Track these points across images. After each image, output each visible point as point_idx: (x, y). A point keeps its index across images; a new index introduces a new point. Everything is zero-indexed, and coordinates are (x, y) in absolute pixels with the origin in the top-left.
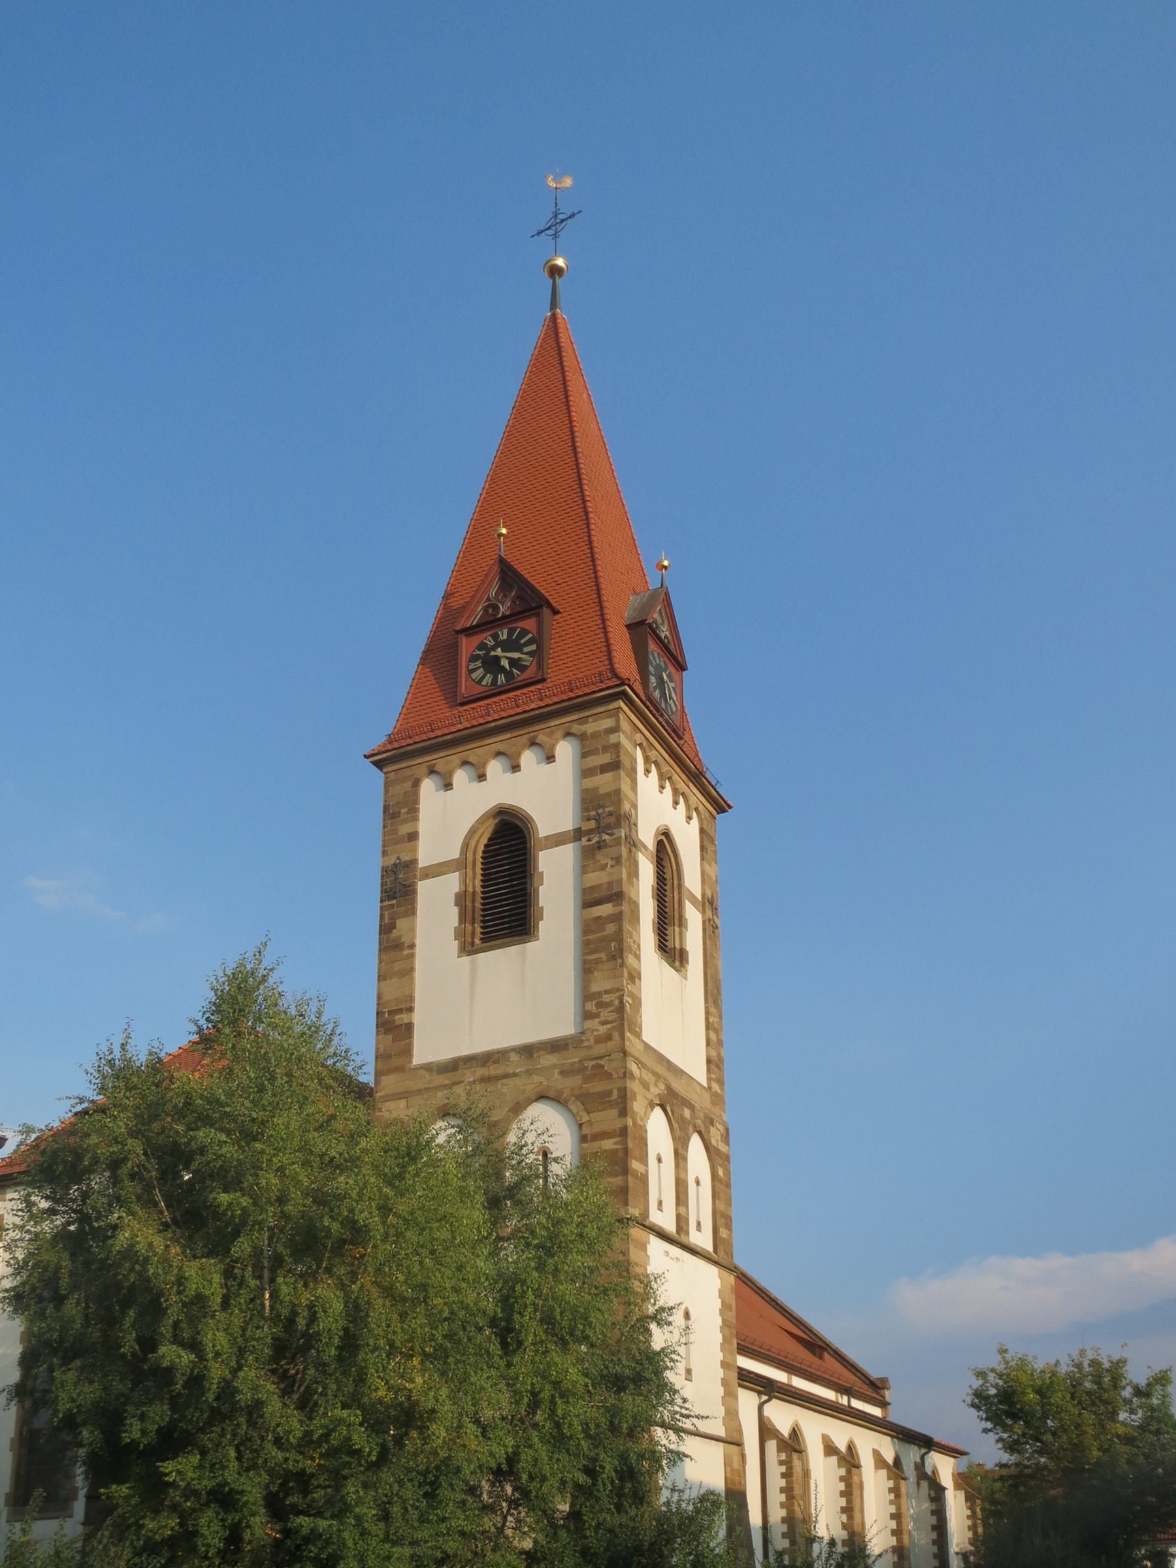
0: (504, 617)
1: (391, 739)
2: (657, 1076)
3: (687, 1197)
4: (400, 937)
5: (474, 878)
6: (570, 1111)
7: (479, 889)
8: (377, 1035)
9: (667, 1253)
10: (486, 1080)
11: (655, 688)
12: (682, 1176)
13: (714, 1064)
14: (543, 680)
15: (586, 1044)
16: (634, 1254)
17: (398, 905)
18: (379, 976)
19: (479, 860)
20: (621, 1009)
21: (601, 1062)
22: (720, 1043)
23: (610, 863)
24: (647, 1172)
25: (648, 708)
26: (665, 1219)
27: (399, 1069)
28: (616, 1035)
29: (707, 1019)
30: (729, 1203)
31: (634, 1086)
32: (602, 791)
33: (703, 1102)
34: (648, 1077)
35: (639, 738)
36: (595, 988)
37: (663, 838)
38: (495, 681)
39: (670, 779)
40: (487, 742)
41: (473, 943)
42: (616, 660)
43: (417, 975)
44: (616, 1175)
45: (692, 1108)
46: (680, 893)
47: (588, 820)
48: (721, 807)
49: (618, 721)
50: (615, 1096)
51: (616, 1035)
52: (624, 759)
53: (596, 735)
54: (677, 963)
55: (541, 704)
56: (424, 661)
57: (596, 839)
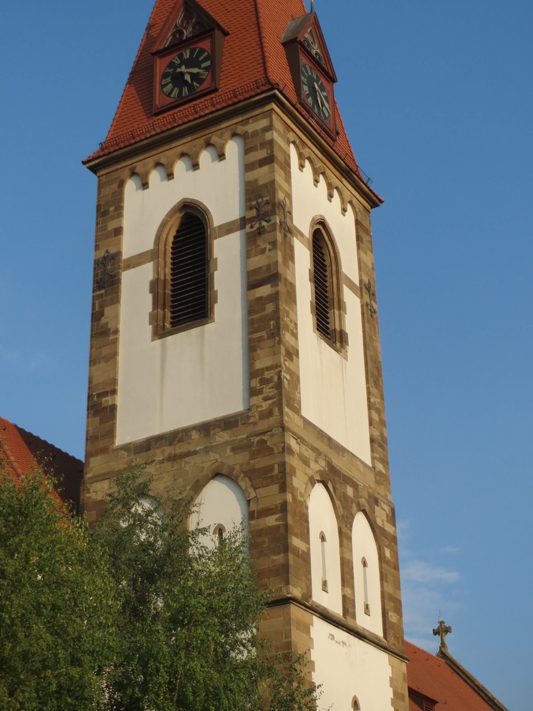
0: (188, 39)
1: (103, 147)
2: (318, 452)
3: (352, 578)
4: (106, 324)
5: (165, 267)
6: (240, 487)
7: (169, 277)
8: (88, 418)
9: (332, 637)
10: (172, 458)
11: (308, 96)
12: (347, 556)
13: (377, 443)
14: (216, 90)
15: (252, 420)
16: (296, 636)
17: (106, 294)
18: (90, 361)
19: (169, 250)
20: (279, 385)
21: (264, 437)
22: (382, 423)
23: (268, 247)
24: (309, 549)
25: (297, 110)
26: (331, 601)
27: (104, 451)
28: (276, 410)
29: (369, 399)
30: (397, 585)
31: (293, 461)
32: (260, 183)
33: (367, 481)
34: (308, 453)
35: (291, 136)
36: (259, 365)
37: (320, 227)
38: (180, 92)
39: (323, 174)
40: (174, 145)
41: (164, 327)
42: (269, 70)
43: (121, 358)
44: (279, 553)
45: (355, 486)
46: (338, 279)
47: (251, 209)
48: (373, 201)
49: (271, 121)
50: (276, 471)
51: (276, 410)
52: (276, 153)
53: (255, 134)
54: (338, 344)
55: (214, 109)
56: (130, 81)
57: (257, 226)
